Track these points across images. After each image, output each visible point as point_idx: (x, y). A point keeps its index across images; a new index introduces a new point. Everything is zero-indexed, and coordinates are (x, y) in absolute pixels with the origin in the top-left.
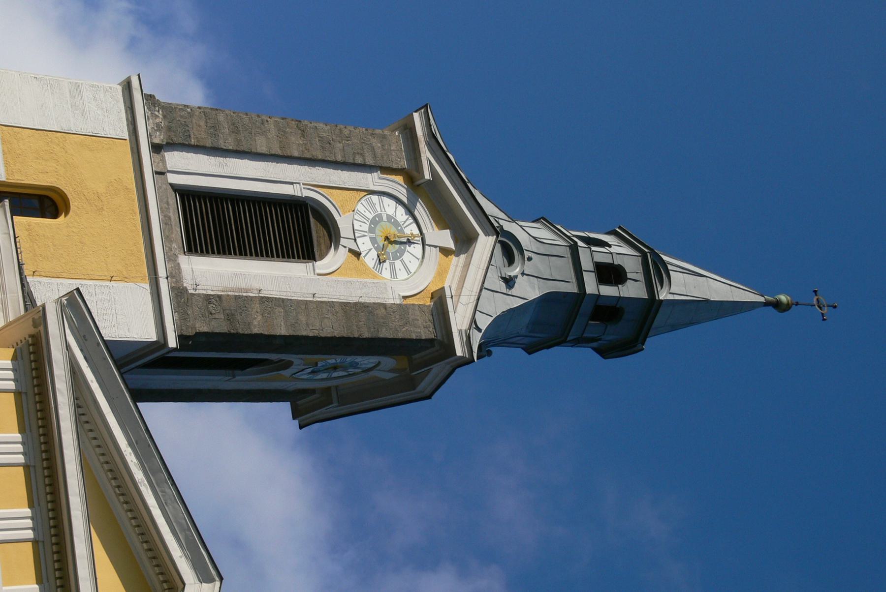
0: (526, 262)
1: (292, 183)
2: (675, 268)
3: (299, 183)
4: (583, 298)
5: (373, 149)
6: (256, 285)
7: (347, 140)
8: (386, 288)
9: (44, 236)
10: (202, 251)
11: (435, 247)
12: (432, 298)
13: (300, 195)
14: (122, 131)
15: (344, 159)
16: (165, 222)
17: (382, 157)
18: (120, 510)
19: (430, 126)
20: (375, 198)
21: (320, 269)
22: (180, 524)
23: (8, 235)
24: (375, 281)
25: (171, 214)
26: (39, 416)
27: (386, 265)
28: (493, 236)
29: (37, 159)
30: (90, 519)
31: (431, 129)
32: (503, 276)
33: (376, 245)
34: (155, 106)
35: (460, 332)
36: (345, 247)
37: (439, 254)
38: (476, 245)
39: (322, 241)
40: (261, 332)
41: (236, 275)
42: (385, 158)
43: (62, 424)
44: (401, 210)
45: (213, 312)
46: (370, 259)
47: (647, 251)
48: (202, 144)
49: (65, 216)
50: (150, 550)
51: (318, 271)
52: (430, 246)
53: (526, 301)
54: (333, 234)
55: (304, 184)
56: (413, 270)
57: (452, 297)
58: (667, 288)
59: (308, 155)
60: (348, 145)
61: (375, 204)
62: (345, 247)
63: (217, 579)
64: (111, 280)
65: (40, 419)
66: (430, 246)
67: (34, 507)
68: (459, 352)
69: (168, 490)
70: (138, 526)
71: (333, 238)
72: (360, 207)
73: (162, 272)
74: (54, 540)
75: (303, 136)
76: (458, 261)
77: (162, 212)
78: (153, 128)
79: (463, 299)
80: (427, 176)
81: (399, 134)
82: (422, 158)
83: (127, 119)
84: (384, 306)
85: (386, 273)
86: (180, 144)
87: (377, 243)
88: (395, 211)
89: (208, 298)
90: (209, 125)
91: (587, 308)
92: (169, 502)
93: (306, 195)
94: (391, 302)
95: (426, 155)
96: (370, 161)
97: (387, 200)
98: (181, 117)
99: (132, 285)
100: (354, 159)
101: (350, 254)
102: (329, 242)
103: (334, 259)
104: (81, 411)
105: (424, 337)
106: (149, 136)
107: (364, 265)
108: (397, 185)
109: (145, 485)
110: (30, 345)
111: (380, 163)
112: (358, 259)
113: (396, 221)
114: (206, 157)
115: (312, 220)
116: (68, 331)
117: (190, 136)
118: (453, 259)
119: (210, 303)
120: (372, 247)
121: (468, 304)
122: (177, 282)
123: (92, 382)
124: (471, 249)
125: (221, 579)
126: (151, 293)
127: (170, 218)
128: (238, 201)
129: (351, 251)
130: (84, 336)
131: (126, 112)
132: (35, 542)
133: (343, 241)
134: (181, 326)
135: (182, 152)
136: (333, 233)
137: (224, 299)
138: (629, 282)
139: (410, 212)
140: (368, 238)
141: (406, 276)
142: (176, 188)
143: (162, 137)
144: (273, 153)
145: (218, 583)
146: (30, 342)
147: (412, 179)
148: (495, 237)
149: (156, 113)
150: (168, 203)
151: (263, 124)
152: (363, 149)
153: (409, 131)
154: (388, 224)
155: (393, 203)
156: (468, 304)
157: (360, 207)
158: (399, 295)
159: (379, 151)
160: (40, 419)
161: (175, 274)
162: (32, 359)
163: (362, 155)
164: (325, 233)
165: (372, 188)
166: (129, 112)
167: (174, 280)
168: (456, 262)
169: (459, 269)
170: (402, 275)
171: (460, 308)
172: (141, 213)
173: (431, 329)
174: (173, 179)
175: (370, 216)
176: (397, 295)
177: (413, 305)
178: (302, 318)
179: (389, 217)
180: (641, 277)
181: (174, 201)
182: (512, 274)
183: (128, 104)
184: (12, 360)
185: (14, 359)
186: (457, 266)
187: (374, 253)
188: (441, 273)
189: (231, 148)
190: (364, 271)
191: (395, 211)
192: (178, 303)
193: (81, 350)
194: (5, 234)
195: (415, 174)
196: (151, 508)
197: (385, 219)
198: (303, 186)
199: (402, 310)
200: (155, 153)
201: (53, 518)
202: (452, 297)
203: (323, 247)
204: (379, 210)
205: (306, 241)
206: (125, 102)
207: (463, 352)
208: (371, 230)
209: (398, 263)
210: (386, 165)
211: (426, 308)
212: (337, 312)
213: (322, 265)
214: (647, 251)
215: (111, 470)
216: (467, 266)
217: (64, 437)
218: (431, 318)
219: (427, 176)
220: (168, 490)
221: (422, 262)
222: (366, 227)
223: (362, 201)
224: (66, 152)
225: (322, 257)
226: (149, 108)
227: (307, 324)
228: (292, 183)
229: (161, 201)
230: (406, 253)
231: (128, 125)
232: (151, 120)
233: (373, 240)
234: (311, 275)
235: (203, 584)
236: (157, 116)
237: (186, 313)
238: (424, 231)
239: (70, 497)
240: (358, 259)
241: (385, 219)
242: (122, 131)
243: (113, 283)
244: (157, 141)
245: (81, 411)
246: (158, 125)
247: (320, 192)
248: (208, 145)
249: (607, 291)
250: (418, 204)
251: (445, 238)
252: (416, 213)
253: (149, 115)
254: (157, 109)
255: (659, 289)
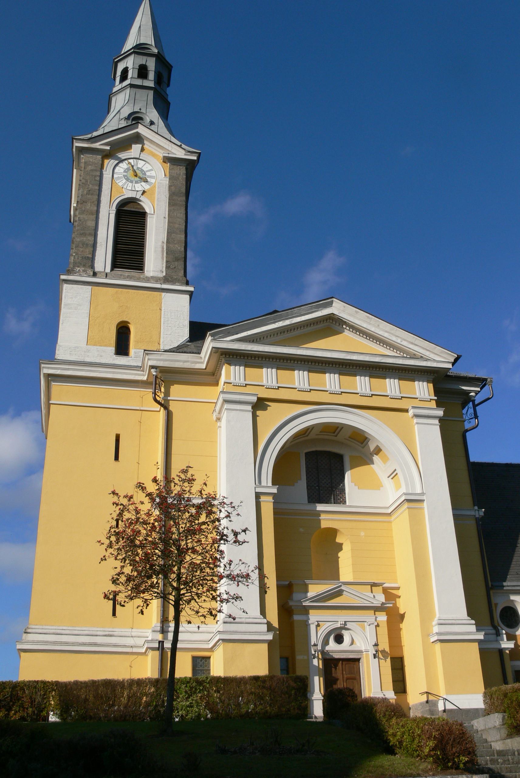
0: (141, 111)
1: (109, 214)
2: (139, 39)
3: (109, 210)
4: (156, 89)
5: (92, 170)
6: (160, 244)
7: (88, 181)
8: (161, 183)
9: (140, 336)
10: (142, 264)
11: (140, 154)
12: (165, 162)
13: (115, 211)
14: (88, 289)
15: (98, 186)
16: (130, 278)
17: (96, 167)
18: (296, 333)
19: (84, 139)
20: (115, 176)
21: (151, 211)
22: (311, 309)
23: (162, 355)
24: (157, 186)
25: (127, 274)
26: (279, 361)
27: (149, 179)
28: (138, 125)
29: (103, 331)
30: (297, 346)
31: (85, 139)
32: (149, 125)
33: (139, 182)
34: (74, 270)
35: (185, 155)
36: (140, 197)
37: (143, 153)
38: (142, 135)
39: (135, 207)
40: (183, 247)
41: (155, 251)
42: (96, 165)
43: (266, 351)
44: (121, 165)
45: (174, 266)
46: (146, 187)
47: (133, 50)
48: (91, 252)
49: (129, 324)
50: (314, 324)
51: (153, 213)
52: (140, 156)
53: (159, 117)
54: (132, 201)
55: (110, 208)
56: (151, 168)
57: (169, 154)
58: (151, 47)
59: (96, 203)
60: (90, 182)
61: (118, 177)
62: (140, 197)
63: (332, 299)
64: (161, 310)
65: (266, 359)
66: (140, 156)
67: (294, 369)
68: (195, 158)
69: (295, 311)
70: (304, 326)
71: (135, 201)
72: (120, 184)
73: (158, 286)
74: (310, 364)
75: (86, 202)
76: (147, 145)
77: (125, 278)
78: (85, 274)
79: (170, 149)
80: (108, 148)
81: (83, 155)
82: (99, 148)
83: (82, 285)
84: (170, 187)
85: (153, 181)
86: (92, 262)
87: (138, 181)
88: (122, 168)
89: (167, 267)
90: (82, 246)
91: (158, 88)
92: (300, 312)
93: (115, 208)
94: (168, 182)
95: (97, 145)
96: (98, 173)
97: (116, 170)
98: (78, 259)
99: (163, 301)
100: (98, 181)
101: (144, 195)
102: (136, 204)
103: (147, 205)
104: (255, 340)
105: (185, 172)
106: (89, 276)
107: (149, 190)
108: (109, 164)
109: (292, 320)
110: (226, 357)
111: (99, 168)
112: (146, 192)
113: (127, 169)
114: (97, 251)
115: (125, 208)
116: (225, 339)
117: (88, 257)
118: (145, 146)
119: (170, 267)
120: (140, 184)
121: (172, 147)
122: (160, 279)
123: (247, 334)
124: (143, 137)
125: (333, 297)
126: (167, 293)
127: (128, 276)
128: (117, 241)
129: (142, 194)
130: (228, 333)
131: (78, 285)
132: (278, 369)
133: (138, 197)
134: (182, 283)
135: (95, 262)
136: (131, 201)
137: (168, 260)
138: (148, 64)
139: (122, 161)
140: (135, 185)
141: (154, 171)
142: (112, 270)
143: (90, 270)
144: (95, 219)
145: (334, 299)
146: (224, 356)
147: (108, 155)
148: (139, 124)
149: (77, 270)
150: (121, 275)
151: (80, 220)
152: (92, 175)
153: (81, 150)
154: (128, 173)
155: (117, 168)
156: (172, 147)
157: (120, 184)
158: (164, 178)
159: (93, 168)
160: (266, 359)
161: (156, 280)
162: (254, 359)
163: (95, 176)
164: (132, 204)
165: (111, 176)
166: (78, 283)
167: (159, 281)
168: (147, 146)
169: (152, 146)
170: (153, 173)
171: (173, 151)
172: (128, 289)
173: (181, 168)
174: (108, 269)
175: (124, 181)
176: (164, 179)
177: (169, 173)
178: (177, 226)
179: (125, 172)
180: (145, 58)
181: (118, 271)
182: (149, 121)
183: (74, 283)
184: (231, 366)
185: (230, 364)
186: (150, 146)
187: (143, 183)
188: (154, 155)
189: (93, 239)
190: (152, 190)
191: (122, 168)
192: (171, 281)
193: (233, 335)
194: (161, 356)
195: (105, 153)
196: (302, 320)
197: (126, 174)
198: (111, 209)
199: (172, 178)
200: (96, 275)
201: (298, 361)
202: (169, 154)
203: (138, 207)
204: (121, 176)
205: (137, 214)
206: (73, 284)
207: (195, 156)
208: (132, 182)
209: (148, 174)
210: (100, 166)
211: (171, 167)
212: (174, 209)
213: (148, 209)
214: (133, 50)
215: (281, 333)
216: (151, 142)
217: (272, 351)
218: (175, 166)
219: (108, 148)
220: (295, 311)
221: (147, 162)
222: (130, 184)
223: (117, 182)
224: (99, 317)
225: (144, 209)
226: (76, 273)
227: (180, 224)
228: (109, 214)
229: (120, 278)
230: (143, 168)
231: (84, 285)
232: (82, 274)
233: (136, 182)
234: (155, 216)
235: (333, 305)
236: (79, 270)
237: (176, 279)
238: (133, 157)
239: (298, 354)
240: (146, 192)
241: (126, 174)
242: (88, 289)
243: (163, 309)
244: (92, 273)
245: (255, 340)
246: (84, 271)
247: (113, 201)
248: (92, 250)
249: (151, 75)
250: (119, 156)
251: (136, 148)
252: (123, 158)
253: (79, 274)
254: (75, 269)
255: (151, 51)
